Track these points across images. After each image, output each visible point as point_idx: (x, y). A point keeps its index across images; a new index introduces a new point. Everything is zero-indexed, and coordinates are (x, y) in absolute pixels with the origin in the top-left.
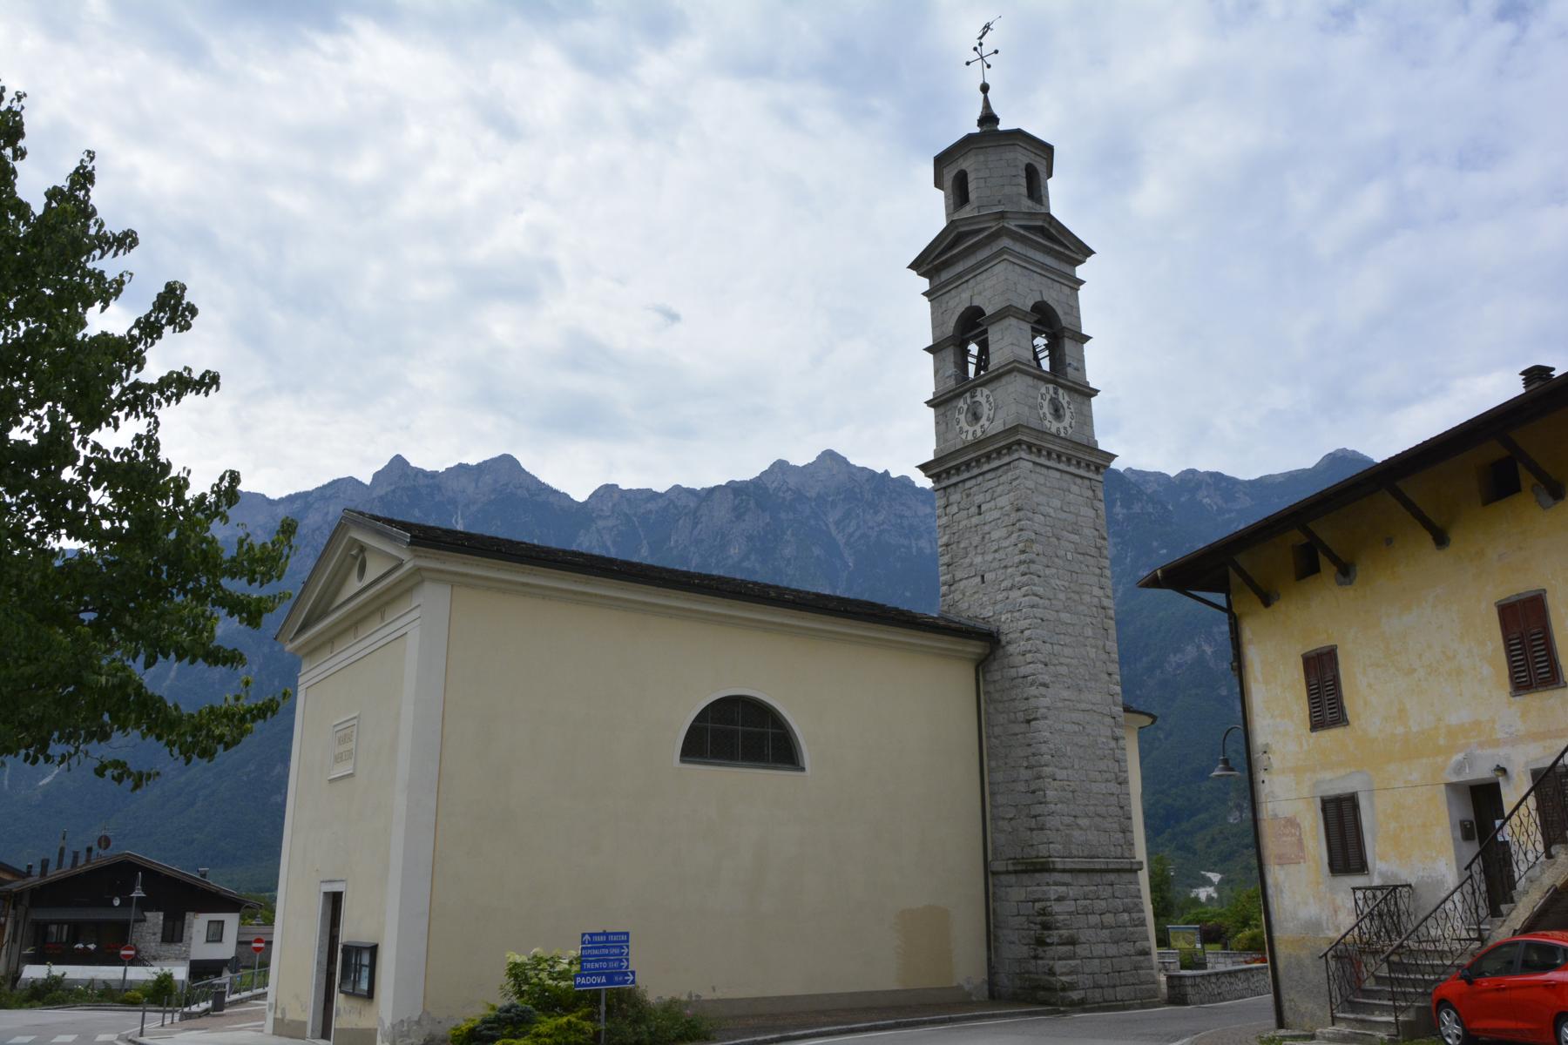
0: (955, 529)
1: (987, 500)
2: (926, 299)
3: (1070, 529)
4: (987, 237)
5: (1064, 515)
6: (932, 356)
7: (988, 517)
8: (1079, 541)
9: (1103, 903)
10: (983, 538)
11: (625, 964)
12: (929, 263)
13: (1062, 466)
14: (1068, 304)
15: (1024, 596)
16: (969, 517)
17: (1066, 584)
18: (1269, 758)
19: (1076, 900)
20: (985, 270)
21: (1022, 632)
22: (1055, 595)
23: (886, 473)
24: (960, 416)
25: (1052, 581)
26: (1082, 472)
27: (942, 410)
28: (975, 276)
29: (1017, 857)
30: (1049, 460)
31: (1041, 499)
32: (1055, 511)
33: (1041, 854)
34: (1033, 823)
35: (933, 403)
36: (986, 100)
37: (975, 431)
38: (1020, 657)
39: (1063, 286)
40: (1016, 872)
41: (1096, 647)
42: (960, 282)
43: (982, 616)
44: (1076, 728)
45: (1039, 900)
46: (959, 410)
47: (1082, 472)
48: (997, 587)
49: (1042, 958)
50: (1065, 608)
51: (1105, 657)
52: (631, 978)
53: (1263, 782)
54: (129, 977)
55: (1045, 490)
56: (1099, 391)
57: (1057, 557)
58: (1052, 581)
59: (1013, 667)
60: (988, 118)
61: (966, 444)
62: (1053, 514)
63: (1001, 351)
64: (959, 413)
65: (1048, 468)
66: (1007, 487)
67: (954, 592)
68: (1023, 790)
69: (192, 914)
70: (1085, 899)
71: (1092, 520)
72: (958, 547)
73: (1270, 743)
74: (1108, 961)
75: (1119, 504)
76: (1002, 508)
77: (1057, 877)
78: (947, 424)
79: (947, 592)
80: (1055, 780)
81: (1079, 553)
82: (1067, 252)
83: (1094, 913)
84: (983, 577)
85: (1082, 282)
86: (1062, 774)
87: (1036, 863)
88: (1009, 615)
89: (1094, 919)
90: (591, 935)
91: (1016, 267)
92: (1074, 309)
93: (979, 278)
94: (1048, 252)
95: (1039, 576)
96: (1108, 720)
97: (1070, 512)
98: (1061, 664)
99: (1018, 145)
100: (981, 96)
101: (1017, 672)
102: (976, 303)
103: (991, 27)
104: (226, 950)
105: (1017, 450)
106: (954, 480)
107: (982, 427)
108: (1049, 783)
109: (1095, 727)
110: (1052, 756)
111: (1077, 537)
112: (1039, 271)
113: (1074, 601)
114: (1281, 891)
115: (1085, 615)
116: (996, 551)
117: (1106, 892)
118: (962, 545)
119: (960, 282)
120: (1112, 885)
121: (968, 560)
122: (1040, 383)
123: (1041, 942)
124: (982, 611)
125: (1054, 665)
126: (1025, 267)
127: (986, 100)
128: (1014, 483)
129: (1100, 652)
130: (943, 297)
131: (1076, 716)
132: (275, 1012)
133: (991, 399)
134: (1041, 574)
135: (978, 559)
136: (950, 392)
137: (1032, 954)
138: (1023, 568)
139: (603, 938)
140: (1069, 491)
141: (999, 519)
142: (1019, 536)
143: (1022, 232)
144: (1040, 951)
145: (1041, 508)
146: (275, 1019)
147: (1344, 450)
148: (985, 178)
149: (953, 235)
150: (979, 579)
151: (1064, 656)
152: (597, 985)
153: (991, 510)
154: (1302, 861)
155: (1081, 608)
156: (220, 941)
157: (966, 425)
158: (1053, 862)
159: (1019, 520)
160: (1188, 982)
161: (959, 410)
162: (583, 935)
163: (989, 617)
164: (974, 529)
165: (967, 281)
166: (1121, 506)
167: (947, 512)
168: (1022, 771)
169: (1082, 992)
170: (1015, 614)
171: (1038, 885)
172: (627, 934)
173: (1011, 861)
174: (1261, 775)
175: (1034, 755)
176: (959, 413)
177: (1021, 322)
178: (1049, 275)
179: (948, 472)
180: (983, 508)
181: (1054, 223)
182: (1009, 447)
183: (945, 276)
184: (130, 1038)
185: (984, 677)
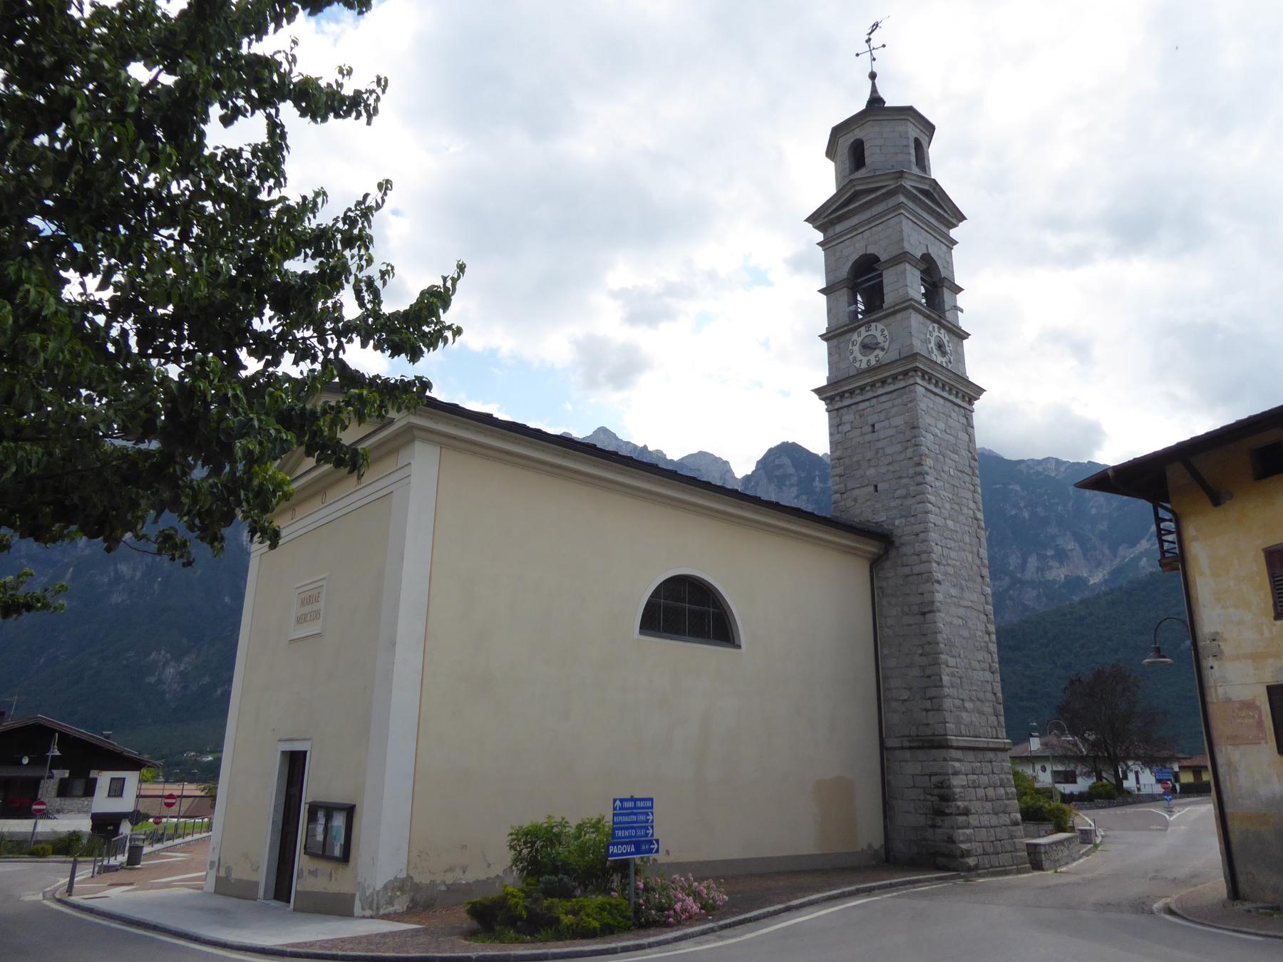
4: (883, 194)
6: (825, 297)
9: (985, 778)
10: (877, 452)
11: (650, 831)
12: (823, 219)
13: (945, 394)
16: (862, 434)
17: (951, 496)
18: (1219, 646)
19: (967, 775)
21: (917, 535)
23: (645, 447)
24: (854, 348)
26: (959, 401)
27: (835, 342)
28: (871, 228)
29: (912, 734)
33: (937, 733)
34: (928, 704)
35: (827, 336)
36: (874, 85)
37: (869, 361)
38: (915, 557)
40: (911, 748)
41: (972, 552)
42: (855, 233)
44: (960, 622)
45: (936, 774)
46: (853, 342)
47: (959, 401)
49: (939, 827)
51: (978, 562)
52: (656, 846)
53: (1212, 668)
54: (39, 829)
55: (934, 414)
60: (875, 101)
64: (853, 345)
65: (935, 394)
69: (96, 771)
70: (973, 774)
73: (1219, 630)
74: (992, 830)
76: (896, 427)
77: (954, 753)
78: (840, 355)
82: (946, 215)
83: (979, 787)
84: (876, 487)
85: (954, 243)
87: (932, 740)
88: (903, 520)
89: (981, 792)
90: (622, 801)
92: (949, 264)
96: (983, 617)
97: (951, 435)
98: (949, 565)
104: (125, 804)
105: (913, 376)
107: (876, 357)
112: (926, 228)
113: (956, 511)
114: (1236, 770)
116: (889, 464)
117: (987, 768)
119: (855, 233)
120: (991, 762)
122: (928, 322)
123: (939, 813)
124: (875, 516)
125: (944, 565)
126: (915, 223)
127: (874, 85)
129: (976, 557)
130: (838, 247)
131: (961, 612)
132: (218, 871)
136: (845, 326)
137: (930, 823)
139: (631, 804)
143: (915, 192)
144: (938, 821)
146: (218, 878)
147: (984, 448)
149: (850, 193)
152: (627, 854)
154: (1263, 741)
155: (961, 518)
156: (121, 795)
158: (950, 740)
160: (1043, 850)
161: (853, 342)
162: (615, 801)
167: (840, 430)
169: (975, 858)
171: (934, 760)
172: (652, 800)
173: (906, 738)
174: (1208, 662)
175: (929, 643)
176: (853, 345)
178: (931, 232)
179: (842, 395)
181: (938, 188)
182: (905, 374)
183: (839, 228)
184: (58, 896)
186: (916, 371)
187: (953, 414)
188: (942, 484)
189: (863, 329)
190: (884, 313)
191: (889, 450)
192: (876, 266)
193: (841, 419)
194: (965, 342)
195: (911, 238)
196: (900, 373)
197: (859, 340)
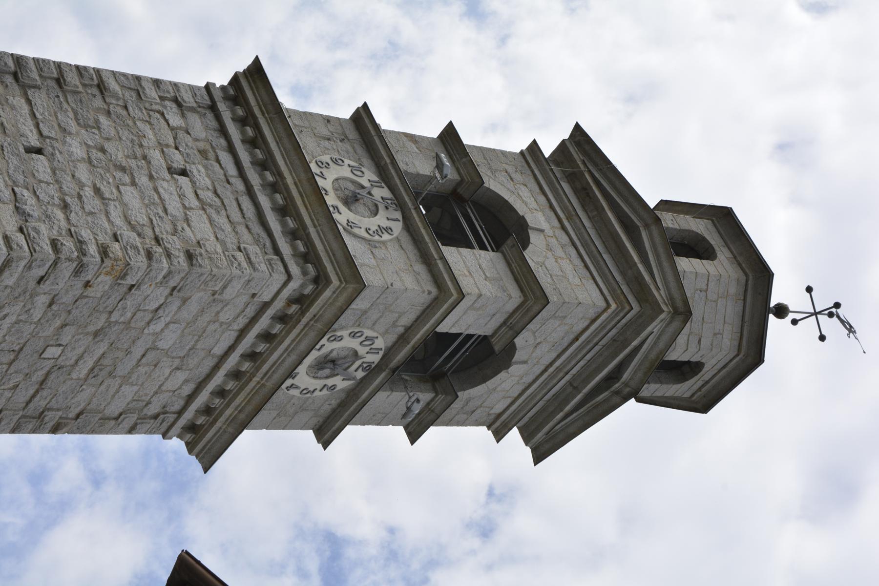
0: (135, 112)
3: (106, 361)
5: (138, 352)
6: (436, 136)
8: (74, 376)
10: (123, 169)
14: (481, 406)
16: (162, 147)
25: (18, 308)
31: (193, 307)
32: (154, 334)
39: (509, 401)
48: (20, 178)
56: (325, 449)
57: (64, 326)
58: (18, 308)
65: (242, 333)
66: (231, 241)
72: (98, 110)
76: (187, 220)
81: (48, 374)
84: (39, 151)
85: (499, 435)
91: (586, 323)
93: (573, 252)
95: (41, 280)
97: (138, 364)
99: (737, 355)
102: (533, 237)
105: (305, 273)
106: (233, 130)
112: (557, 364)
116: (97, 191)
121: (73, 127)
122: (392, 338)
128: (240, 256)
133: (386, 237)
134: (46, 286)
138: (68, 244)
140: (177, 369)
141: (165, 210)
142: (136, 248)
143: (635, 343)
145: (177, 303)
150: (34, 141)
153: (182, 196)
157: (335, 176)
159: (169, 255)
165: (563, 228)
177: (505, 316)
180: (182, 180)
181: (616, 399)
186: (316, 281)
187: (181, 376)
188: (37, 314)
189: (386, 193)
191: (129, 193)
193: (192, 109)
194: (310, 434)
195: (558, 323)
196: (309, 243)
197: (364, 182)
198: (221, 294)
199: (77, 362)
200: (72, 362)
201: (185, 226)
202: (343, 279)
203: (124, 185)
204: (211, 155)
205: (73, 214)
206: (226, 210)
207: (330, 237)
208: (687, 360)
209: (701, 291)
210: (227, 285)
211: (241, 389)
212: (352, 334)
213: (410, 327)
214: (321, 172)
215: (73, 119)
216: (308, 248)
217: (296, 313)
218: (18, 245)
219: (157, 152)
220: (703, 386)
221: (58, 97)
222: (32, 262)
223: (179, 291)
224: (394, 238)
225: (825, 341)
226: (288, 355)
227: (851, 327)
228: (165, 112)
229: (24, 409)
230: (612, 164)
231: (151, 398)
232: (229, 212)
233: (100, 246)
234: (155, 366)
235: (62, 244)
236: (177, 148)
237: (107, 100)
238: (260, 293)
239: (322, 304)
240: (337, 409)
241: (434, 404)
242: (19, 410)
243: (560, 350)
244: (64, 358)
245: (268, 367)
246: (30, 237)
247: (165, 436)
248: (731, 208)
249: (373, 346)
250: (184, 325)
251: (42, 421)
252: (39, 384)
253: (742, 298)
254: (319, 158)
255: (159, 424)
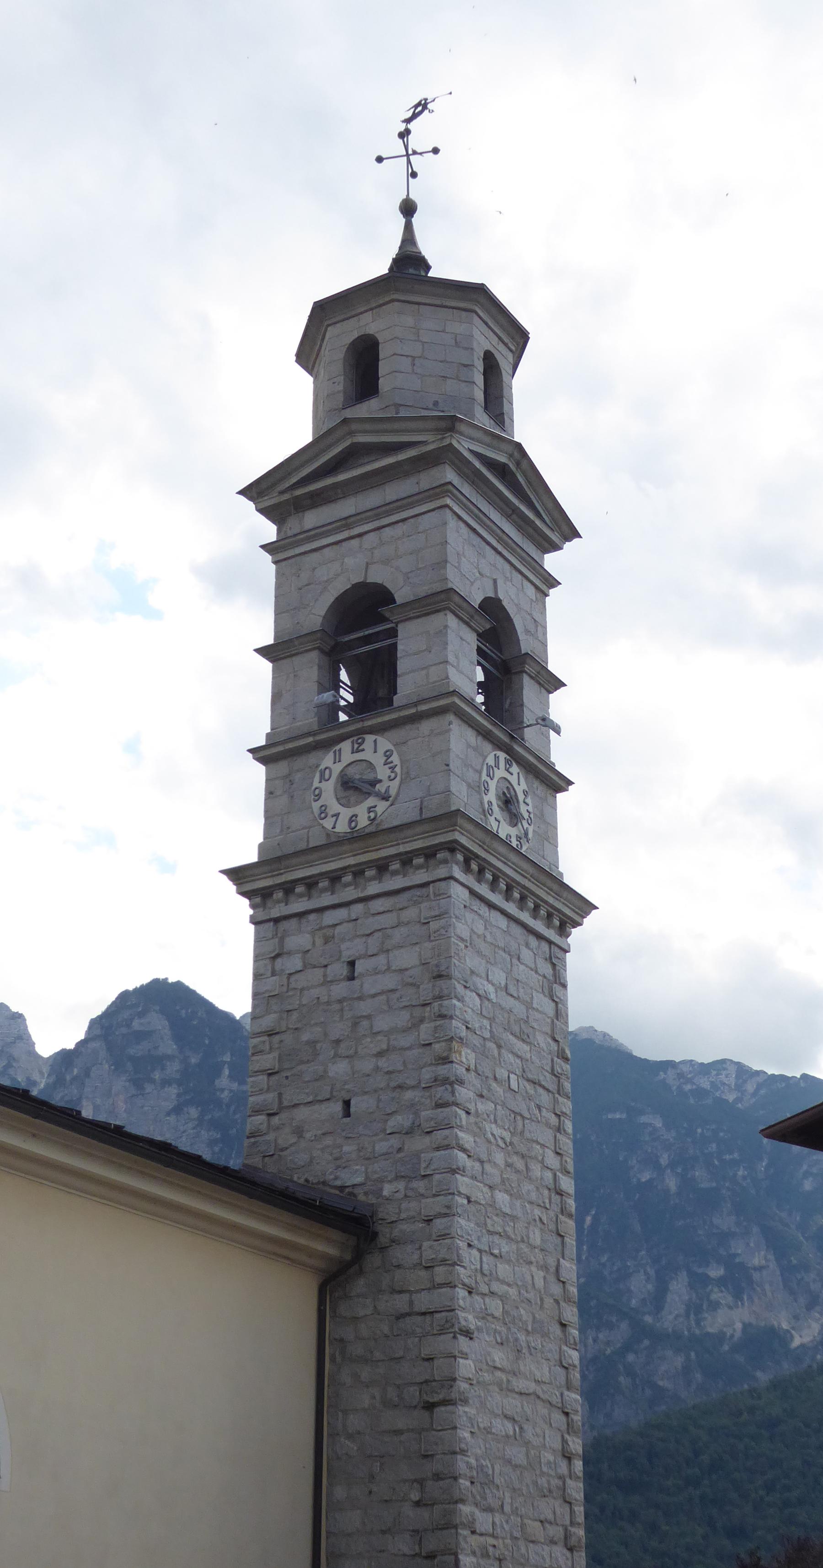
1: (370, 953)
2: (268, 558)
5: (510, 1002)
7: (369, 985)
8: (528, 1056)
15: (438, 1149)
16: (327, 982)
17: (507, 1135)
20: (403, 520)
21: (429, 1221)
22: (489, 1154)
27: (283, 767)
30: (493, 891)
36: (409, 228)
37: (353, 818)
39: (526, 583)
41: (545, 1267)
43: (338, 1183)
44: (509, 1427)
50: (503, 1181)
51: (556, 1289)
55: (483, 946)
59: (400, 1292)
61: (333, 839)
62: (492, 996)
63: (424, 672)
64: (322, 778)
65: (491, 906)
67: (278, 1128)
68: (406, 1550)
71: (549, 1020)
75: (226, 1072)
76: (402, 971)
79: (264, 1127)
80: (473, 1532)
81: (528, 1080)
82: (538, 522)
84: (347, 1104)
85: (552, 582)
86: (483, 1521)
88: (401, 1185)
94: (511, 513)
95: (468, 1113)
96: (558, 1418)
97: (517, 998)
100: (400, 221)
101: (411, 1303)
103: (429, 106)
105: (445, 861)
106: (298, 906)
107: (370, 810)
108: (465, 1537)
109: (538, 1430)
110: (472, 1483)
111: (526, 1048)
112: (494, 542)
113: (517, 1171)
115: (531, 1203)
116: (380, 1054)
118: (305, 1037)
122: (487, 747)
127: (409, 228)
128: (434, 925)
129: (552, 1278)
131: (513, 1404)
133: (395, 759)
134: (471, 1107)
135: (339, 1069)
140: (519, 959)
141: (392, 991)
147: (592, 1029)
148: (414, 358)
150: (337, 1108)
151: (498, 1279)
153: (376, 972)
155: (527, 1187)
157: (334, 801)
163: (354, 1186)
164: (337, 1007)
166: (230, 1076)
168: (408, 1511)
170: (415, 1184)
175: (437, 1477)
176: (322, 778)
177: (464, 626)
179: (288, 889)
180: (359, 967)
181: (524, 465)
182: (430, 854)
183: (312, 519)
185: (334, 1310)
186: (452, 850)
189: (346, 746)
190: (394, 716)
192: (385, 611)
198: (466, 941)
199: (518, 1057)
200: (518, 1061)
201: (407, 973)
202: (452, 828)
203: (371, 1027)
204: (329, 932)
205: (408, 1082)
206: (386, 928)
207: (409, 832)
208: (483, 376)
209: (414, 365)
210: (460, 937)
211: (533, 894)
212: (486, 791)
213: (477, 731)
214: (333, 816)
215: (308, 1065)
216: (420, 854)
217: (477, 862)
218: (444, 1139)
219: (332, 987)
220: (503, 342)
221: (287, 1077)
222: (458, 1126)
223: (466, 982)
224: (395, 748)
225: (439, 148)
226: (509, 861)
227: (419, 104)
228: (288, 972)
229: (553, 1093)
230: (283, 462)
231: (540, 975)
232: (388, 926)
233: (437, 1063)
234: (518, 981)
235: (440, 1099)
236: (326, 966)
237: (284, 1029)
238: (462, 902)
239: (471, 843)
240: (540, 779)
241: (533, 673)
242: (554, 1097)
243: (484, 544)
244: (517, 1070)
245: (518, 875)
246: (436, 1127)
247: (566, 951)
248: (315, 303)
249: (493, 766)
250: (489, 966)
251: (561, 1074)
252: (536, 1086)
253: (417, 306)
254: (316, 814)
255: (560, 961)
